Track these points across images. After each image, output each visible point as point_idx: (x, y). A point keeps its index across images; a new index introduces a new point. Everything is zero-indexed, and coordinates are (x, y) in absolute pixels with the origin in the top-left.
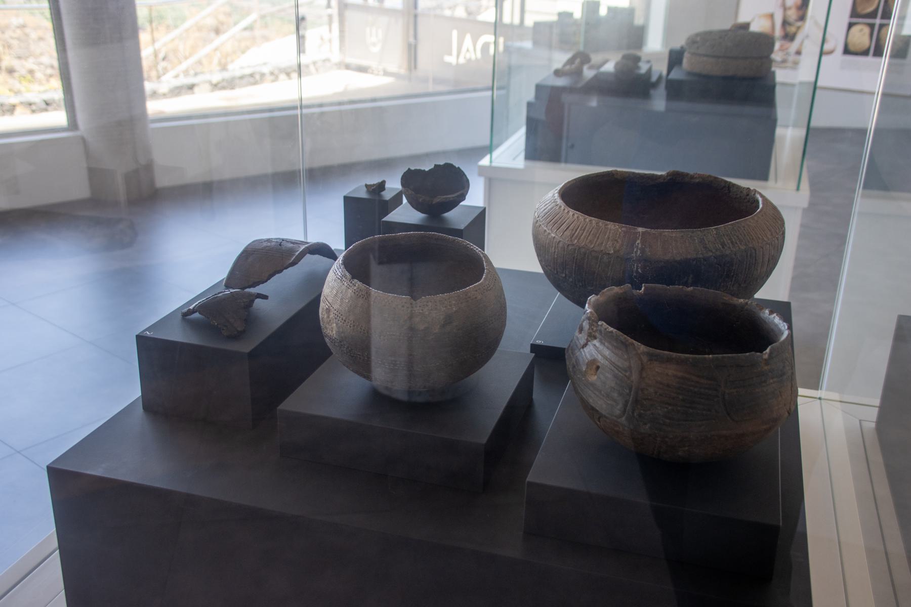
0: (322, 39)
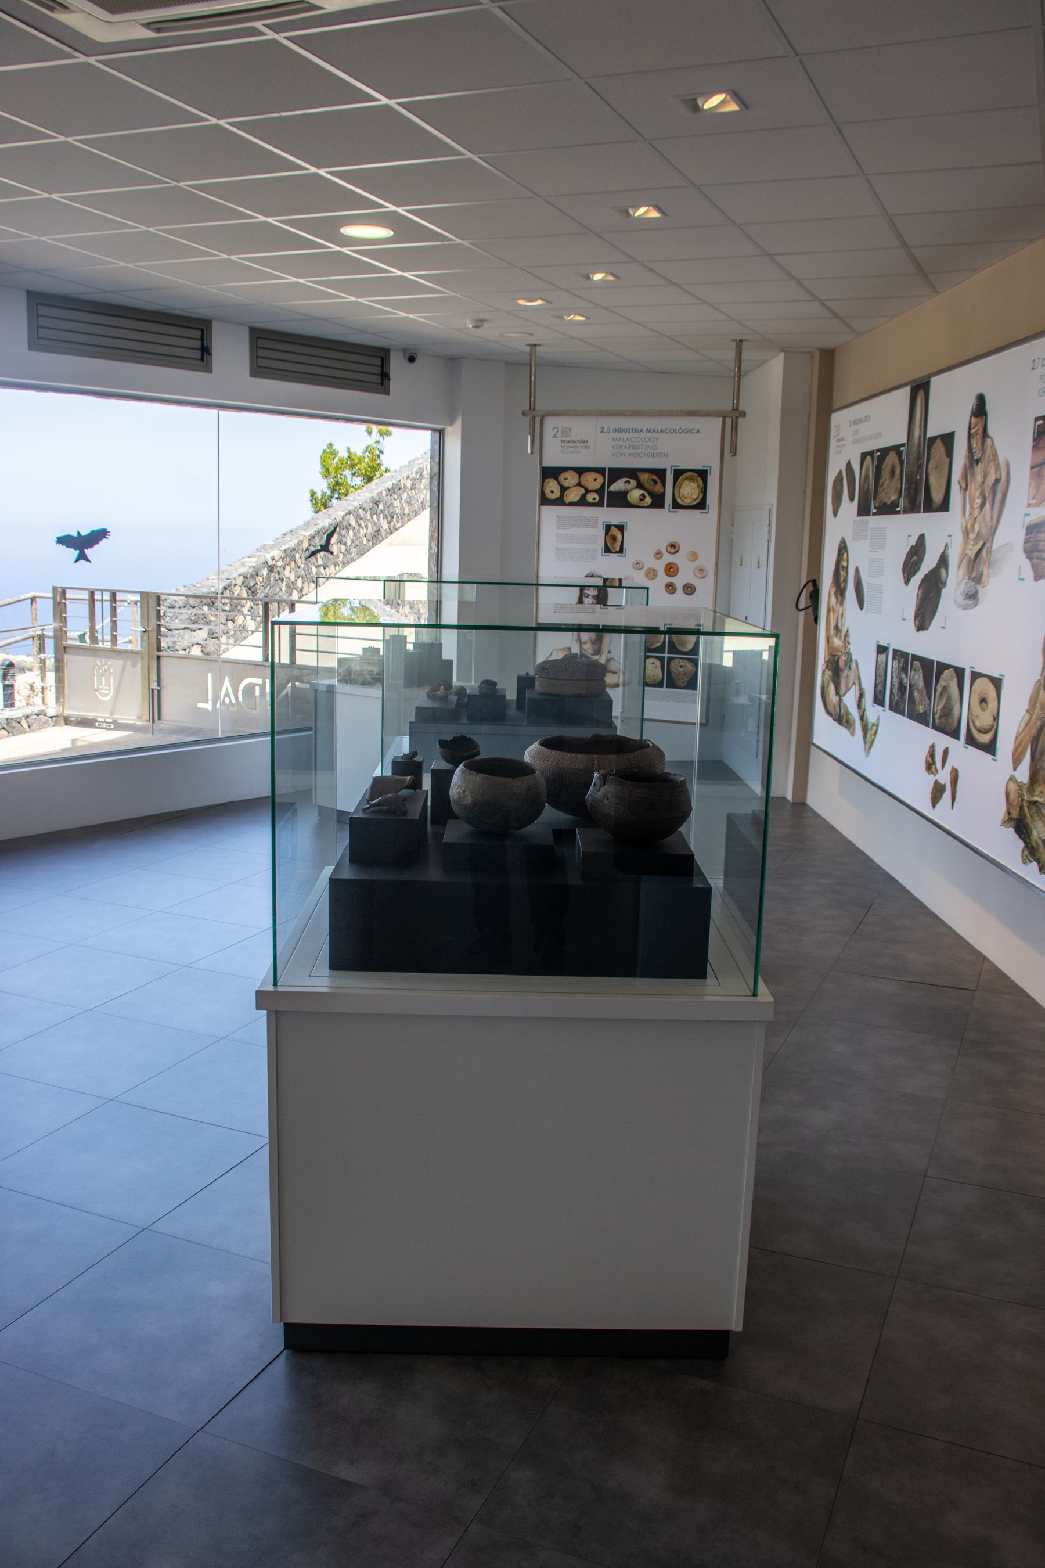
0: (32, 687)
